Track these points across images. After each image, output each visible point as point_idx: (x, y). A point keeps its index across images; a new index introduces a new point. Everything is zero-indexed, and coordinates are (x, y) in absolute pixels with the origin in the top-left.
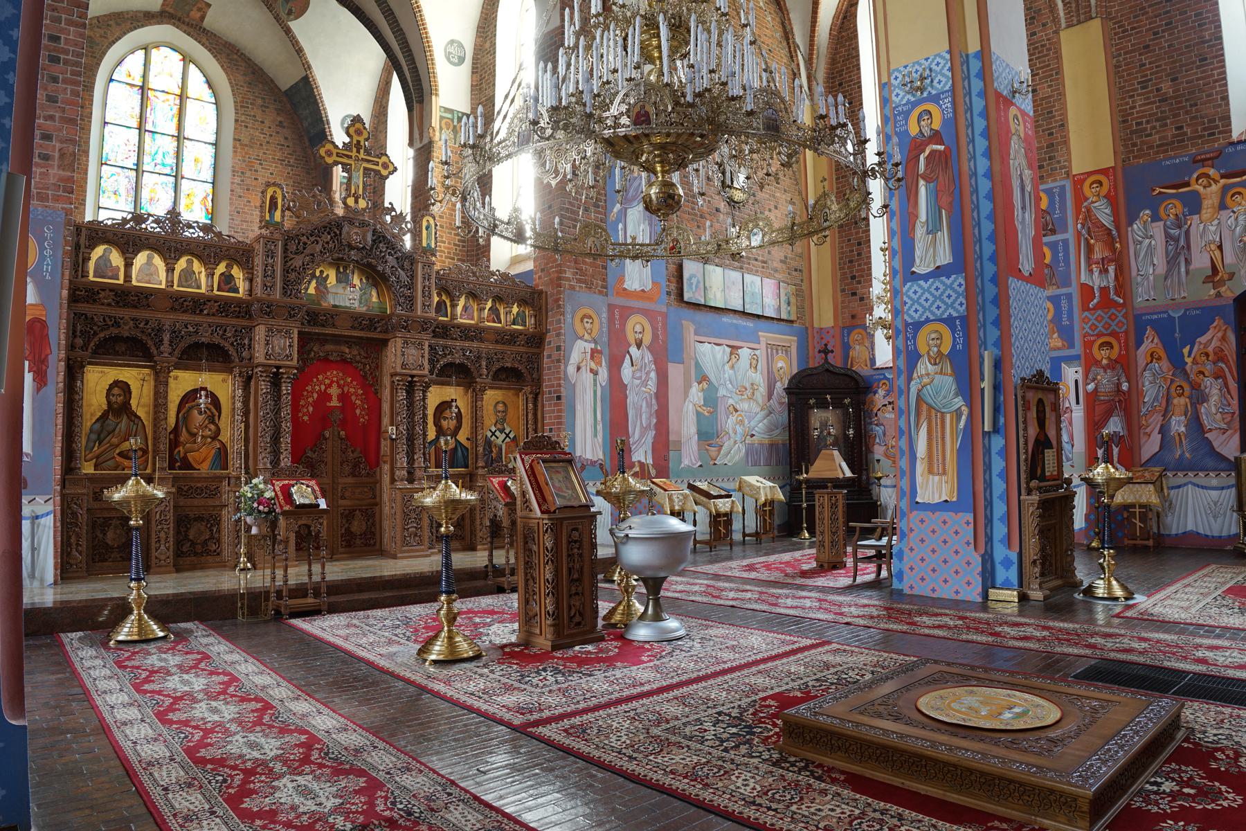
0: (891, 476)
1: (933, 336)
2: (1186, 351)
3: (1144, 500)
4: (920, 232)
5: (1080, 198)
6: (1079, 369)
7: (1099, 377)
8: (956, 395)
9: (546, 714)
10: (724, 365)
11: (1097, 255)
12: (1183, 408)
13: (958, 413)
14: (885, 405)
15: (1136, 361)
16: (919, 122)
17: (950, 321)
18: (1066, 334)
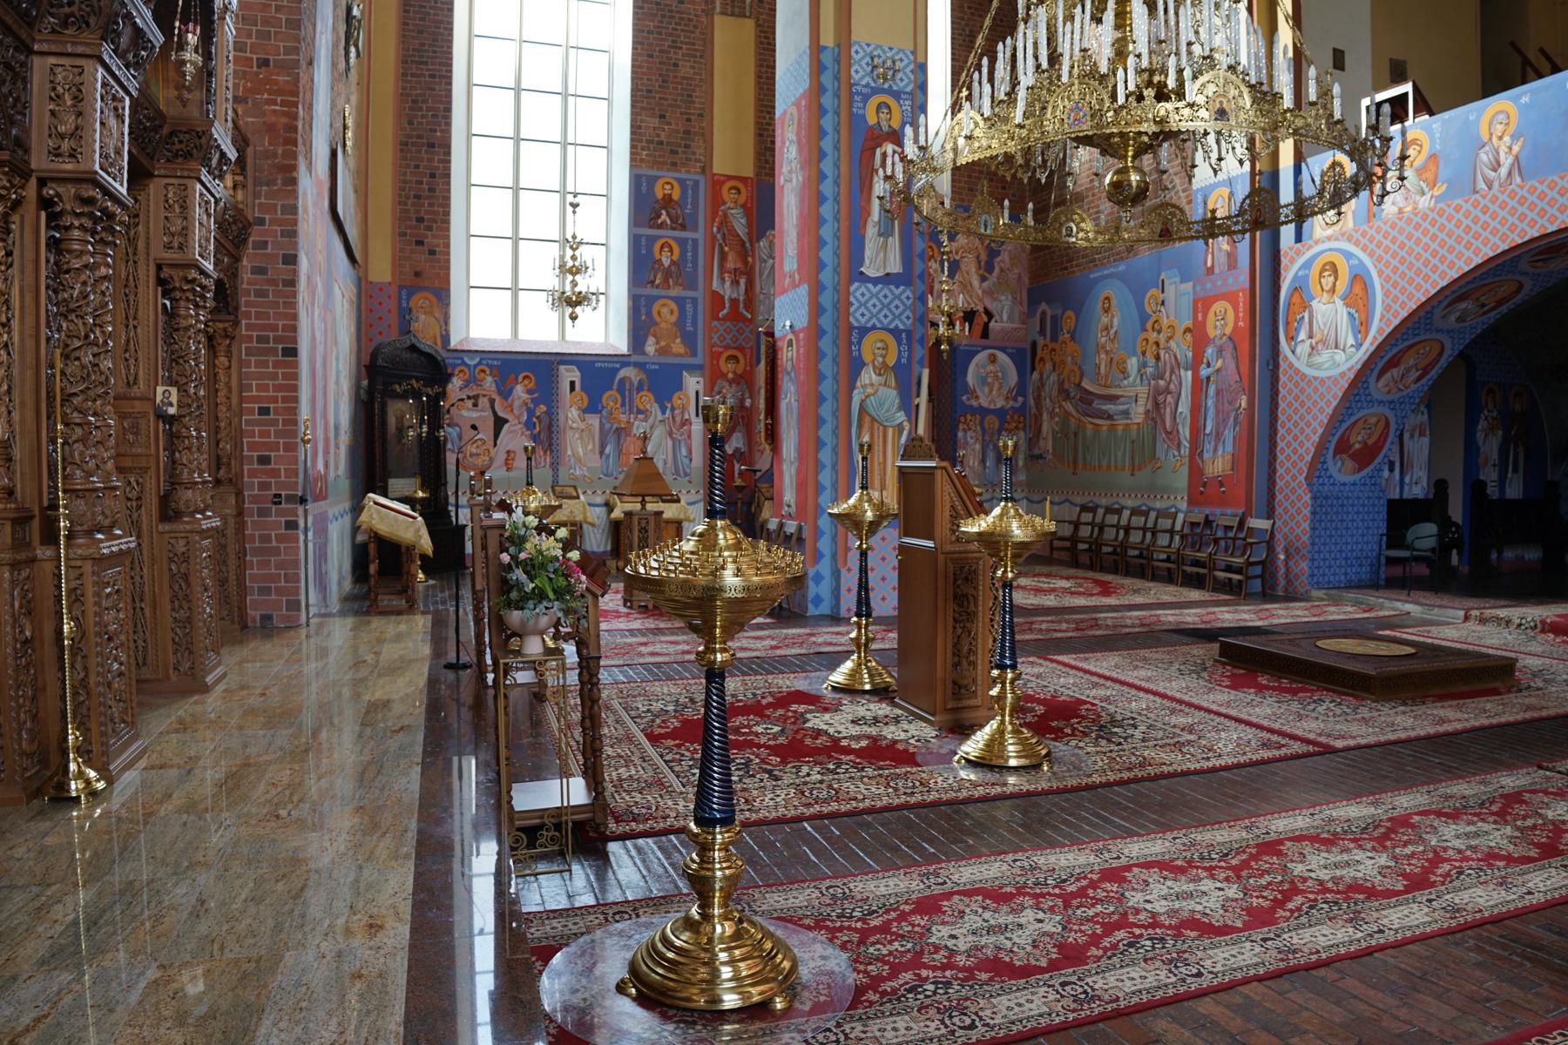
0: (599, 492)
1: (879, 345)
4: (871, 231)
5: (716, 201)
6: (701, 379)
8: (899, 409)
9: (1151, 770)
11: (730, 265)
13: (900, 428)
14: (462, 400)
16: (878, 112)
17: (895, 332)
18: (689, 340)
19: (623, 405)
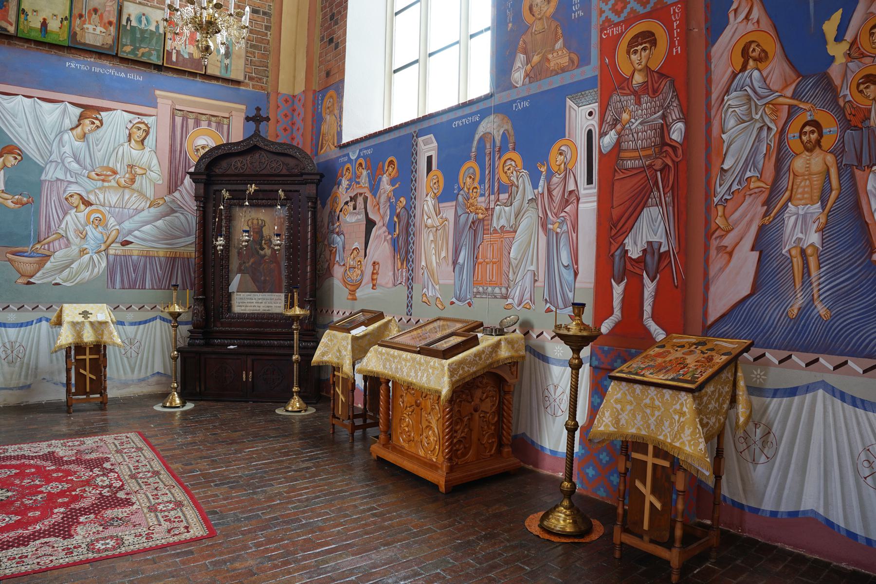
2: (830, 27)
3: (665, 436)
7: (625, 116)
10: (61, 133)
12: (817, 181)
15: (708, 70)
19: (481, 182)
